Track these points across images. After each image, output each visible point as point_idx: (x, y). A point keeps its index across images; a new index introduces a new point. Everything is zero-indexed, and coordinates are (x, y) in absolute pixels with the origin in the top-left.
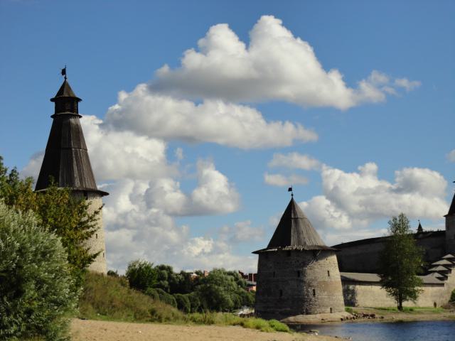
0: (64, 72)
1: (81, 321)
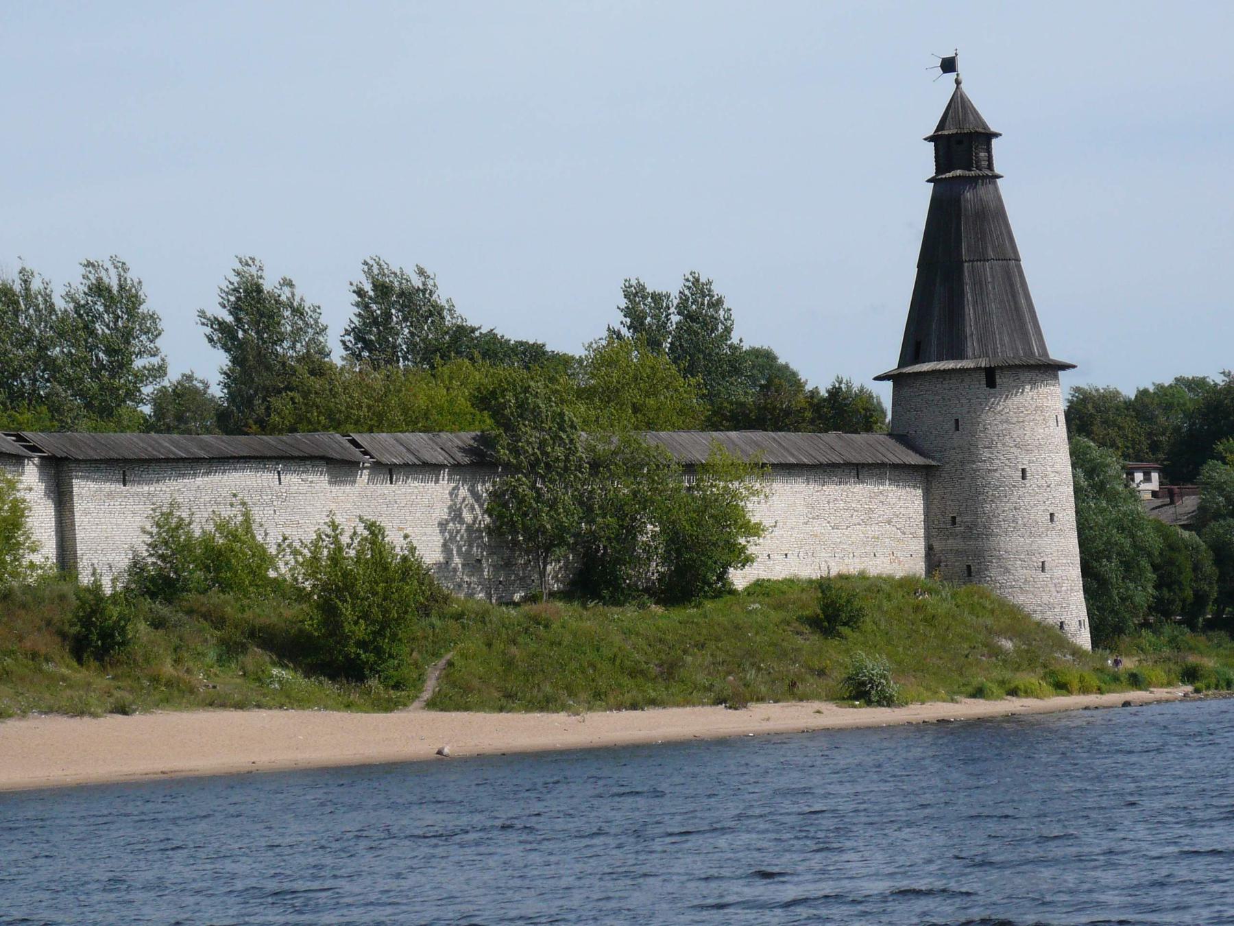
0: (948, 65)
1: (119, 717)
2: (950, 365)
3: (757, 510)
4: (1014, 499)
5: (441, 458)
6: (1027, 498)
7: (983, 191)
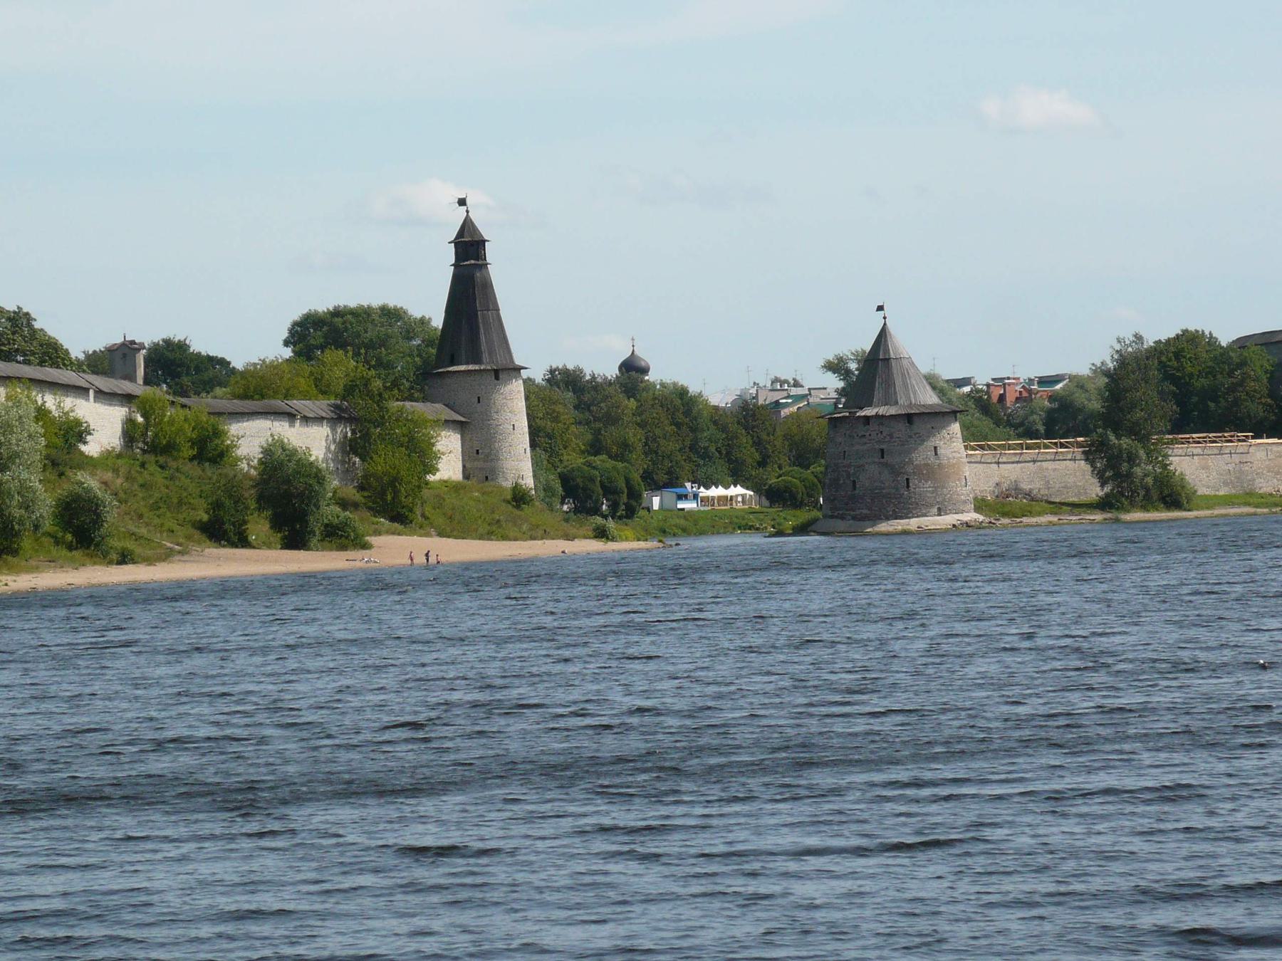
2: (471, 367)
5: (324, 415)
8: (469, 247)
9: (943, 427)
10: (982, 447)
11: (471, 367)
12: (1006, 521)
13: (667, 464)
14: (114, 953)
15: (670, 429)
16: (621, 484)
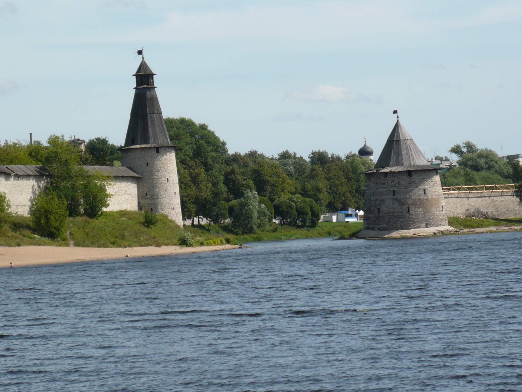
0: (140, 52)
1: (18, 247)
2: (143, 146)
3: (109, 190)
4: (165, 187)
5: (31, 173)
6: (169, 187)
7: (152, 92)
8: (144, 78)
9: (429, 178)
10: (459, 189)
11: (143, 146)
12: (466, 230)
13: (342, 198)
14: (286, 387)
15: (344, 181)
16: (308, 210)
